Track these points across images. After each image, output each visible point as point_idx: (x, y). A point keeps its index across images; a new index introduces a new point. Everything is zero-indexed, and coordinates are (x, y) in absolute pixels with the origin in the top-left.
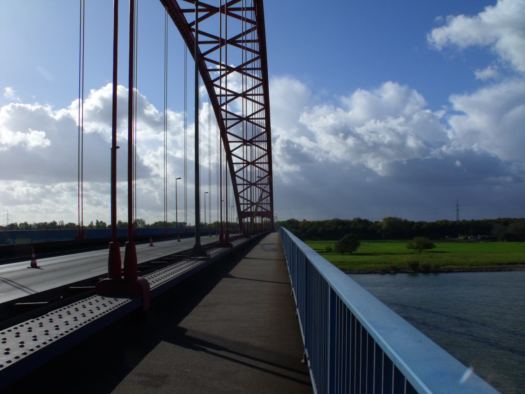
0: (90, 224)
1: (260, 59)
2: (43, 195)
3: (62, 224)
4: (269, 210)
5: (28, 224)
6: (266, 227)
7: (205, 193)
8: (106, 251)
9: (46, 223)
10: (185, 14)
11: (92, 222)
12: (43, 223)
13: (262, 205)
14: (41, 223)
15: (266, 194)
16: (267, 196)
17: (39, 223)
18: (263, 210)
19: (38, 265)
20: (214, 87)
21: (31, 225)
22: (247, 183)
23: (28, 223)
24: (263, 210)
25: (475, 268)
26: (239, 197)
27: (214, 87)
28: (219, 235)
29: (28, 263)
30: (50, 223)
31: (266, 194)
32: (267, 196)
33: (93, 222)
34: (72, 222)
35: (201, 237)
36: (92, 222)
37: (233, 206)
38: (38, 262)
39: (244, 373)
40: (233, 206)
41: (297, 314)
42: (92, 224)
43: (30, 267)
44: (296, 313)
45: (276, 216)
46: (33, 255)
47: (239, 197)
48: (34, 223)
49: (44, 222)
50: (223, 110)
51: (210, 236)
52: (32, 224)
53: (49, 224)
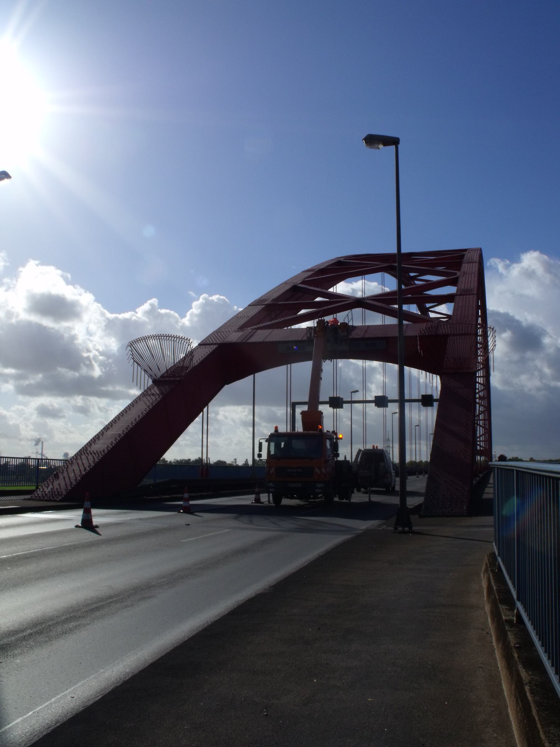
2: (158, 395)
5: (167, 461)
7: (415, 426)
9: (189, 460)
10: (253, 375)
11: (247, 460)
12: (185, 460)
13: (480, 443)
17: (181, 459)
18: (482, 448)
19: (96, 521)
20: (429, 312)
21: (170, 462)
23: (166, 460)
24: (482, 448)
25: (18, 478)
26: (95, 529)
27: (429, 312)
28: (427, 476)
29: (76, 516)
30: (194, 459)
33: (248, 460)
34: (222, 460)
35: (409, 477)
36: (247, 460)
37: (419, 425)
38: (95, 516)
39: (497, 681)
40: (419, 425)
41: (499, 564)
42: (247, 462)
44: (497, 563)
45: (495, 454)
46: (257, 490)
47: (95, 529)
48: (175, 460)
51: (418, 477)
52: (173, 461)
53: (193, 461)
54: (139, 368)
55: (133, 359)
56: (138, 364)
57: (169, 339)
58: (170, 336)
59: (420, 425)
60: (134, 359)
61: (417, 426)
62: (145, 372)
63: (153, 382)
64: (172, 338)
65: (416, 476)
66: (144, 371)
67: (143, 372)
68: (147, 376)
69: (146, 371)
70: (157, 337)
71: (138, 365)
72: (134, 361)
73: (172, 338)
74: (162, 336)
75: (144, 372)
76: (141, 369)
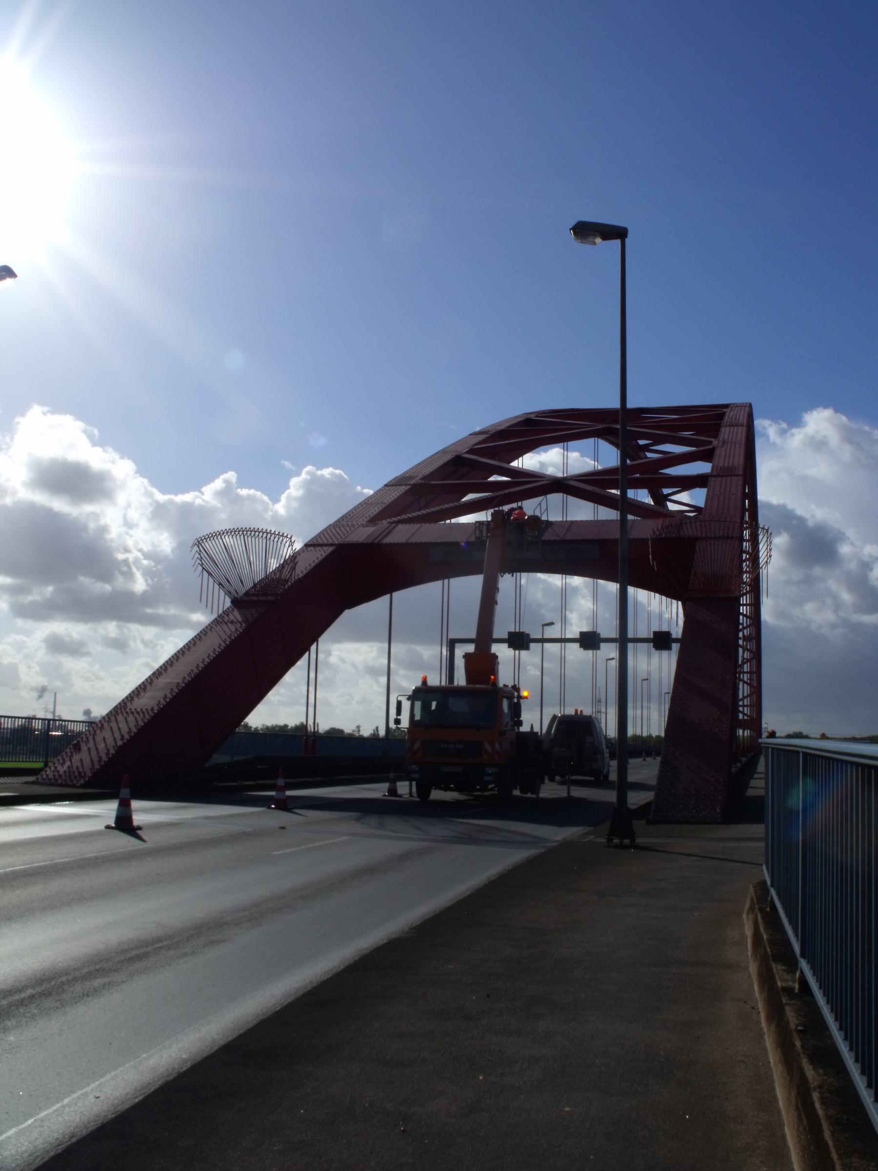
0: (372, 732)
1: (747, 531)
3: (316, 730)
4: (755, 717)
5: (251, 727)
6: (27, 723)
7: (642, 680)
8: (367, 789)
9: (286, 726)
11: (377, 728)
13: (743, 709)
14: (276, 726)
15: (743, 611)
16: (745, 597)
17: (272, 725)
21: (256, 729)
22: (624, 493)
24: (746, 717)
28: (659, 759)
31: (743, 611)
32: (748, 624)
33: (379, 729)
36: (377, 728)
37: (647, 679)
43: (114, 825)
46: (392, 775)
48: (263, 725)
49: (282, 724)
50: (741, 712)
52: (260, 727)
53: (292, 728)
54: (211, 581)
55: (202, 566)
56: (210, 574)
57: (258, 535)
58: (264, 531)
59: (649, 678)
60: (204, 566)
61: (645, 680)
62: (220, 587)
63: (232, 602)
64: (263, 534)
65: (652, 758)
66: (219, 585)
67: (217, 587)
68: (222, 593)
69: (222, 586)
70: (241, 533)
71: (209, 575)
72: (203, 568)
73: (263, 534)
74: (248, 531)
75: (218, 587)
76: (214, 581)
